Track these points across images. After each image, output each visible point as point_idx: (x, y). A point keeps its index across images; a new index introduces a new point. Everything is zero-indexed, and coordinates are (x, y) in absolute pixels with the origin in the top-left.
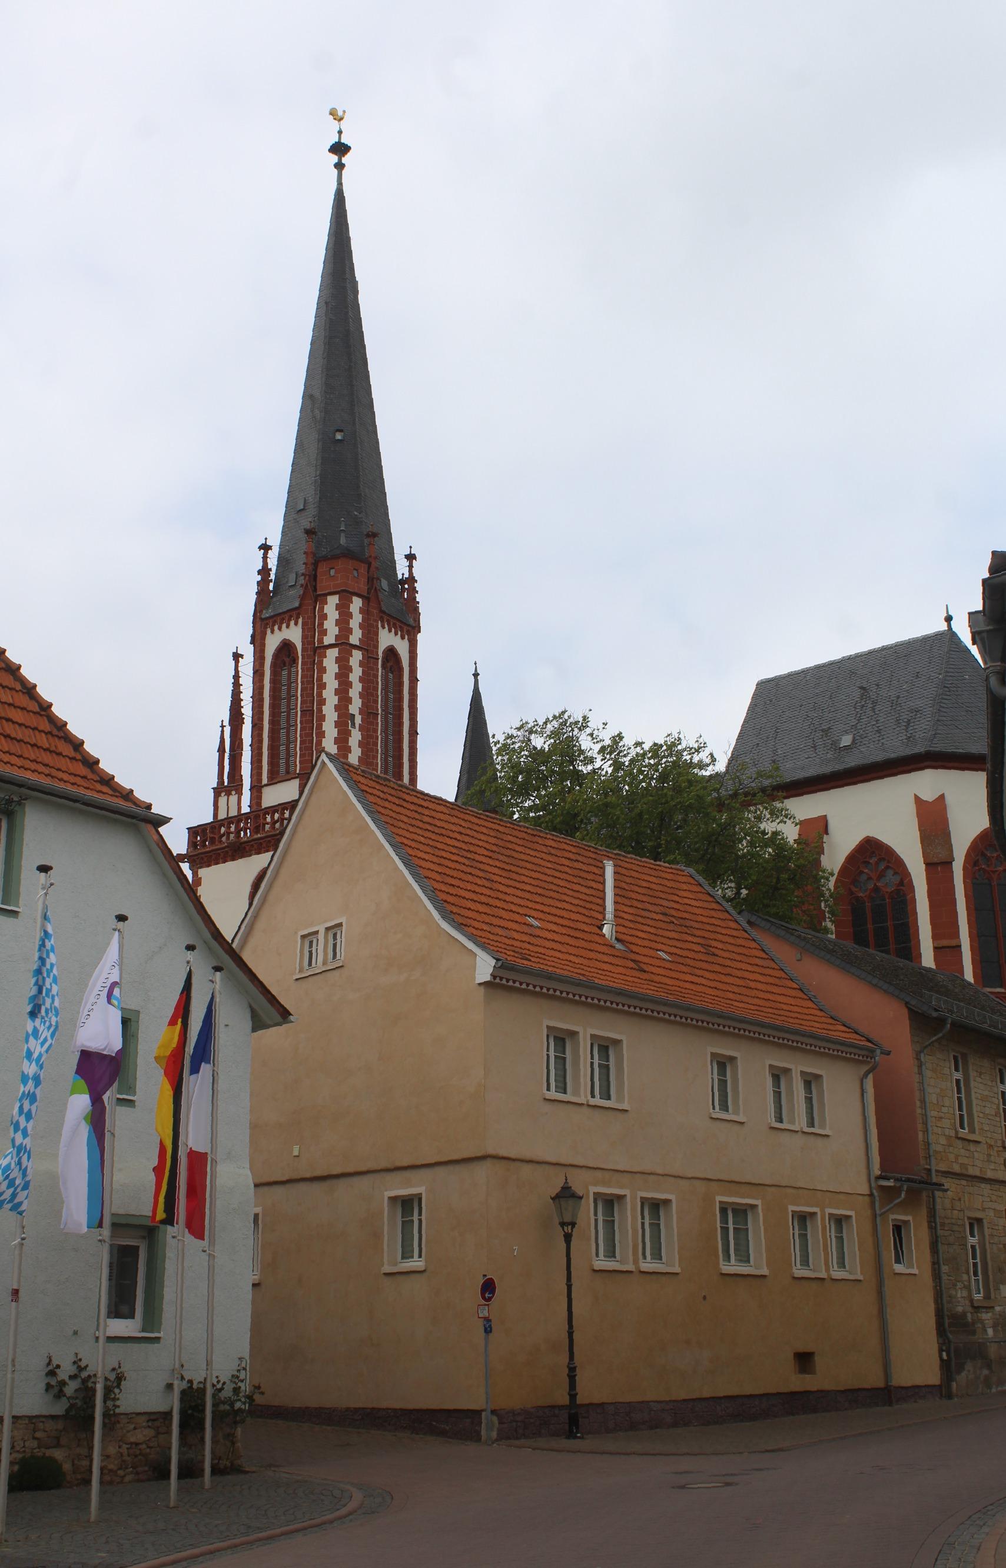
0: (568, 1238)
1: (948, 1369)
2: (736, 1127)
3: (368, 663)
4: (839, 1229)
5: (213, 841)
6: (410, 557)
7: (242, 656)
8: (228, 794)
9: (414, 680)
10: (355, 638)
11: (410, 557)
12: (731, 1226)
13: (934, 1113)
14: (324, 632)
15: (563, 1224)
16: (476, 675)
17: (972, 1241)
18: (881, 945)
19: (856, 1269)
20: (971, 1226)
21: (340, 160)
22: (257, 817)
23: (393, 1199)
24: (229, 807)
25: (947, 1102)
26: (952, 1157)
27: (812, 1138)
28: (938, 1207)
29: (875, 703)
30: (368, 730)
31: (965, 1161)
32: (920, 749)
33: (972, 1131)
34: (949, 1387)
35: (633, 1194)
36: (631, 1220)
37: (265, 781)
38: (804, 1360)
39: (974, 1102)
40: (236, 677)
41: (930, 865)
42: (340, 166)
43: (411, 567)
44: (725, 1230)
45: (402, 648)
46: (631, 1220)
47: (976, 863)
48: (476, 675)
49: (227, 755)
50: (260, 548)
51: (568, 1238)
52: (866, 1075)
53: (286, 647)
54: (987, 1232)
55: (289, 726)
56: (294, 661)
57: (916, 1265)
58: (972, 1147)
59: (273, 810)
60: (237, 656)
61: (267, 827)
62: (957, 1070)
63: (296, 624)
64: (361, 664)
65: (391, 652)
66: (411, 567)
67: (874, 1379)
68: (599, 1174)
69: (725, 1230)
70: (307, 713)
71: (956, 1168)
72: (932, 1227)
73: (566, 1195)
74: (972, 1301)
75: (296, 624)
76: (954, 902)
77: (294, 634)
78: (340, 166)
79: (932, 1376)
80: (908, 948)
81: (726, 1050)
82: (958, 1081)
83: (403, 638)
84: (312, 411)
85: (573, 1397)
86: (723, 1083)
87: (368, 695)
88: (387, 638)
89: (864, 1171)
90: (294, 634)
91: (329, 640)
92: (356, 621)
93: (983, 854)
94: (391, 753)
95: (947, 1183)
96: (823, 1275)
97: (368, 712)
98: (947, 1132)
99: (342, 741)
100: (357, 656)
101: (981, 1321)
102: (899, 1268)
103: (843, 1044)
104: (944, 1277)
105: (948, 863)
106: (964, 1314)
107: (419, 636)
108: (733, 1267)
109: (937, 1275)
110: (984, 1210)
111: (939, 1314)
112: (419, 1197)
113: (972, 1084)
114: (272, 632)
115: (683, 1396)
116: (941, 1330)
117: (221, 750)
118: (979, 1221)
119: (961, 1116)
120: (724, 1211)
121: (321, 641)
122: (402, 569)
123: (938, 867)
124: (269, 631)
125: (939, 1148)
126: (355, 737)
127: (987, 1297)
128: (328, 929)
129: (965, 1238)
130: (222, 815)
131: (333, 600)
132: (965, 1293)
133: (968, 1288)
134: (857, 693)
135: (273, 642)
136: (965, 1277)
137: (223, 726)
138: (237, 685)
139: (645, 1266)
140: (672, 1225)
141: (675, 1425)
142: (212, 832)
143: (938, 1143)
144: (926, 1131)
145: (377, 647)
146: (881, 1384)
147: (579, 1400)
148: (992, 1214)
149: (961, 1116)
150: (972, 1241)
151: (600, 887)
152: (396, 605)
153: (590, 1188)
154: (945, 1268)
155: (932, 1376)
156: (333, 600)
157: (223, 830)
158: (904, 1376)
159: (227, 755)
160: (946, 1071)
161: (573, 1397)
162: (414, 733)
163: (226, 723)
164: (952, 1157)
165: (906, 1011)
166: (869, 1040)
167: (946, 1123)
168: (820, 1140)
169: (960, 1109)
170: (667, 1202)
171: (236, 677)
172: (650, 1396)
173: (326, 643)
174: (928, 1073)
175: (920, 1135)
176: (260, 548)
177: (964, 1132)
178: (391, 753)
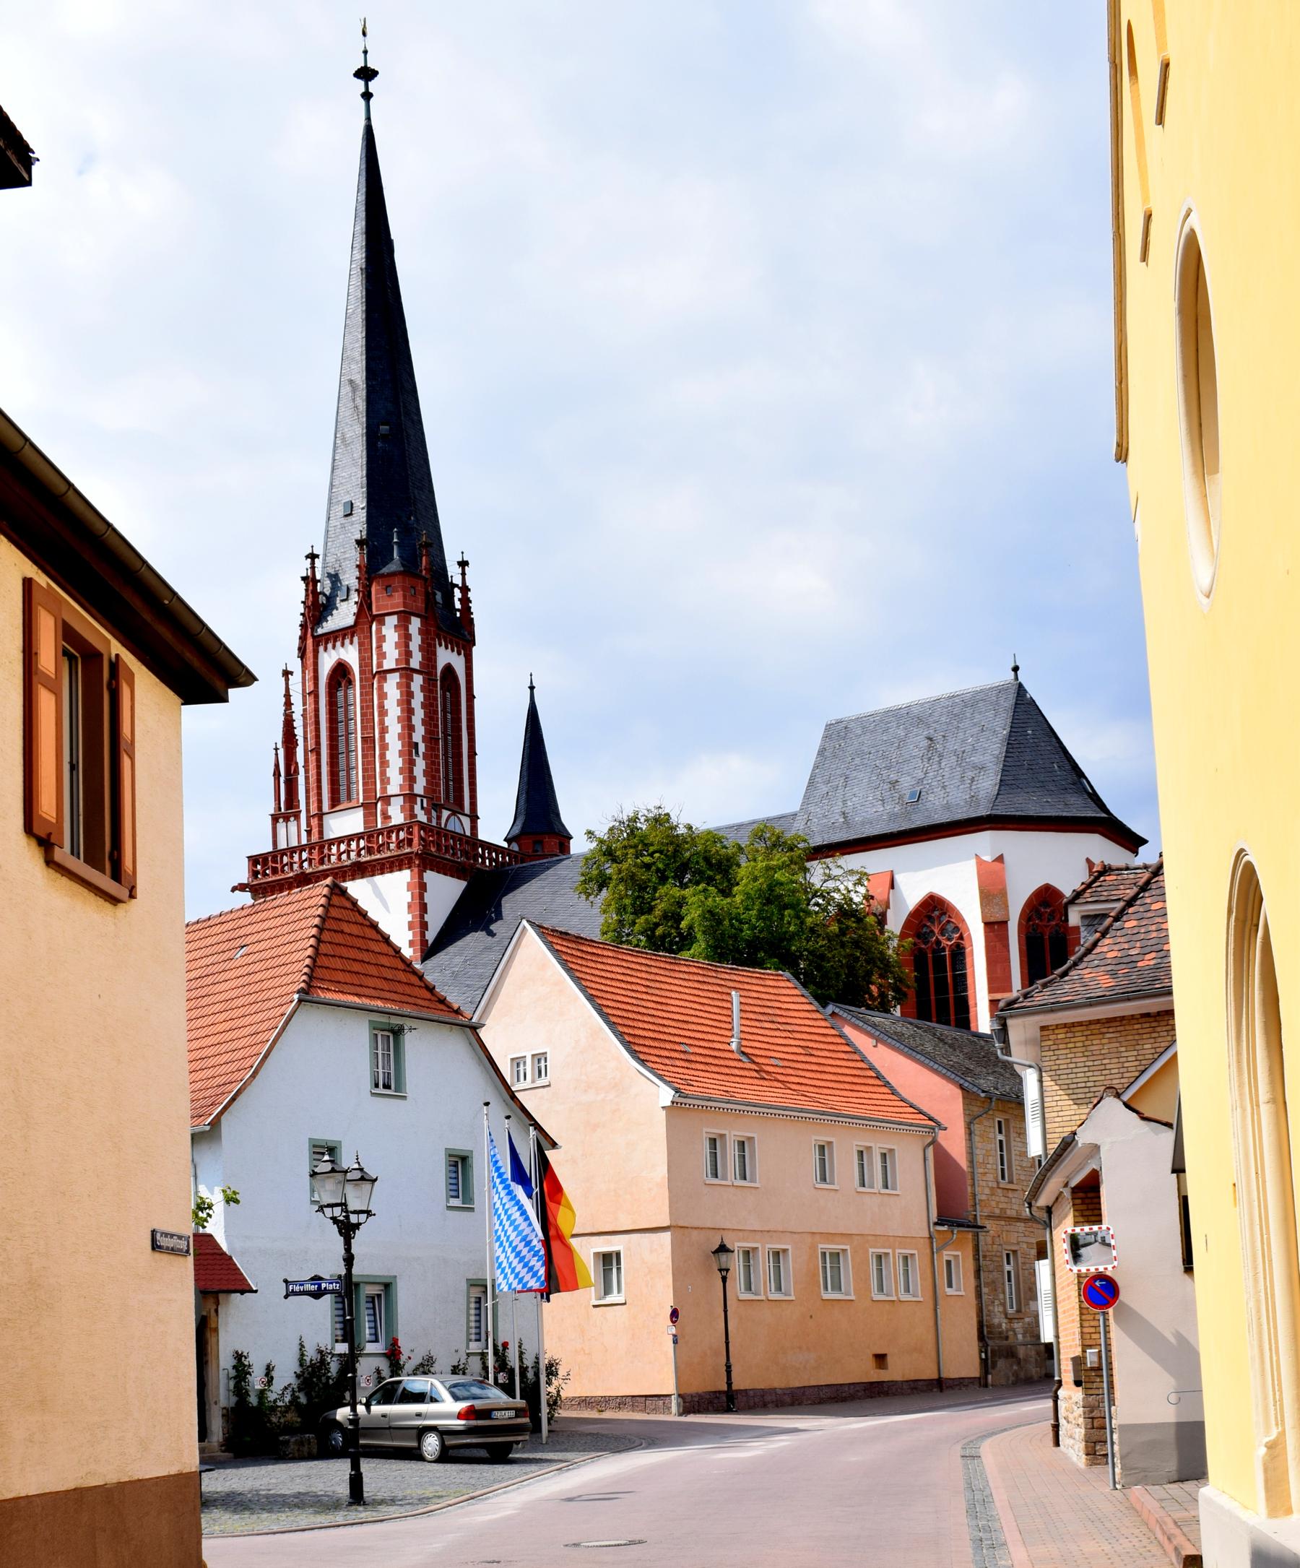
0: (724, 1279)
1: (986, 1365)
2: (833, 1193)
3: (428, 688)
4: (906, 1264)
5: (275, 871)
6: (463, 564)
7: (291, 673)
8: (287, 819)
9: (471, 697)
10: (415, 662)
11: (463, 564)
12: (828, 1265)
13: (981, 1170)
14: (382, 655)
15: (720, 1270)
16: (532, 688)
17: (1007, 1268)
18: (943, 1020)
19: (920, 1291)
20: (1008, 1255)
21: (367, 86)
22: (322, 848)
23: (596, 1254)
24: (291, 834)
25: (991, 1160)
26: (993, 1204)
27: (886, 1198)
28: (981, 1243)
29: (941, 756)
30: (431, 757)
31: (1004, 1206)
32: (983, 812)
33: (1011, 1182)
34: (986, 1378)
35: (764, 1249)
36: (763, 1264)
37: (326, 808)
38: (880, 1359)
39: (1013, 1157)
40: (287, 696)
41: (988, 925)
42: (367, 96)
43: (463, 574)
44: (825, 1268)
45: (458, 664)
46: (763, 1264)
47: (1029, 919)
48: (532, 688)
49: (282, 779)
50: (307, 557)
51: (724, 1279)
52: (929, 1145)
53: (341, 671)
54: (1020, 1260)
55: (348, 752)
56: (350, 683)
57: (963, 1287)
58: (1010, 1194)
59: (339, 840)
60: (287, 674)
61: (333, 859)
62: (1000, 1132)
63: (351, 643)
64: (423, 689)
65: (449, 669)
66: (463, 574)
67: (930, 1374)
68: (741, 1234)
69: (825, 1268)
70: (368, 741)
71: (997, 1211)
72: (976, 1259)
73: (723, 1249)
74: (1006, 1314)
75: (351, 643)
76: (1008, 960)
77: (350, 654)
78: (367, 96)
79: (973, 1370)
80: (962, 1015)
81: (824, 1138)
82: (1001, 1142)
83: (459, 654)
84: (354, 400)
85: (729, 1384)
86: (823, 1161)
87: (429, 721)
88: (445, 656)
89: (925, 1219)
90: (350, 654)
91: (389, 664)
92: (416, 641)
93: (1038, 911)
94: (451, 777)
95: (989, 1224)
96: (894, 1298)
97: (430, 738)
98: (990, 1184)
99: (408, 771)
100: (418, 680)
101: (1014, 1330)
102: (949, 1291)
103: (911, 1125)
104: (985, 1297)
105: (1004, 924)
106: (1000, 1325)
107: (475, 650)
108: (831, 1295)
109: (979, 1295)
110: (1018, 1243)
111: (981, 1325)
112: (618, 1254)
113: (1013, 1143)
114: (326, 649)
115: (797, 1385)
116: (981, 1337)
117: (277, 774)
118: (1015, 1252)
119: (1003, 1170)
120: (824, 1254)
121: (380, 665)
122: (454, 573)
123: (995, 928)
124: (321, 649)
125: (984, 1197)
126: (420, 765)
127: (1019, 1311)
128: (533, 1056)
129: (1002, 1266)
130: (282, 845)
131: (392, 621)
132: (1001, 1309)
133: (1004, 1305)
134: (926, 743)
135: (327, 660)
136: (1001, 1296)
137: (276, 749)
138: (288, 704)
139: (772, 1297)
140: (790, 1266)
141: (792, 1404)
142: (275, 861)
143: (983, 1193)
144: (973, 1185)
145: (435, 667)
146: (935, 1376)
147: (734, 1387)
148: (1025, 1246)
149: (1003, 1170)
150: (1007, 1268)
151: (728, 1005)
152: (450, 622)
153: (737, 1245)
154: (985, 1290)
155: (973, 1370)
156: (392, 621)
157: (285, 859)
158: (950, 1372)
159: (282, 779)
160: (991, 1135)
161: (729, 1384)
162: (472, 754)
163: (280, 745)
164: (993, 1204)
165: (958, 1092)
166: (931, 1119)
167: (990, 1177)
168: (892, 1199)
169: (1002, 1164)
170: (785, 1251)
171: (287, 696)
172: (776, 1385)
173: (386, 667)
174: (977, 1139)
175: (969, 1189)
176: (307, 557)
177: (1003, 1184)
178: (451, 777)
